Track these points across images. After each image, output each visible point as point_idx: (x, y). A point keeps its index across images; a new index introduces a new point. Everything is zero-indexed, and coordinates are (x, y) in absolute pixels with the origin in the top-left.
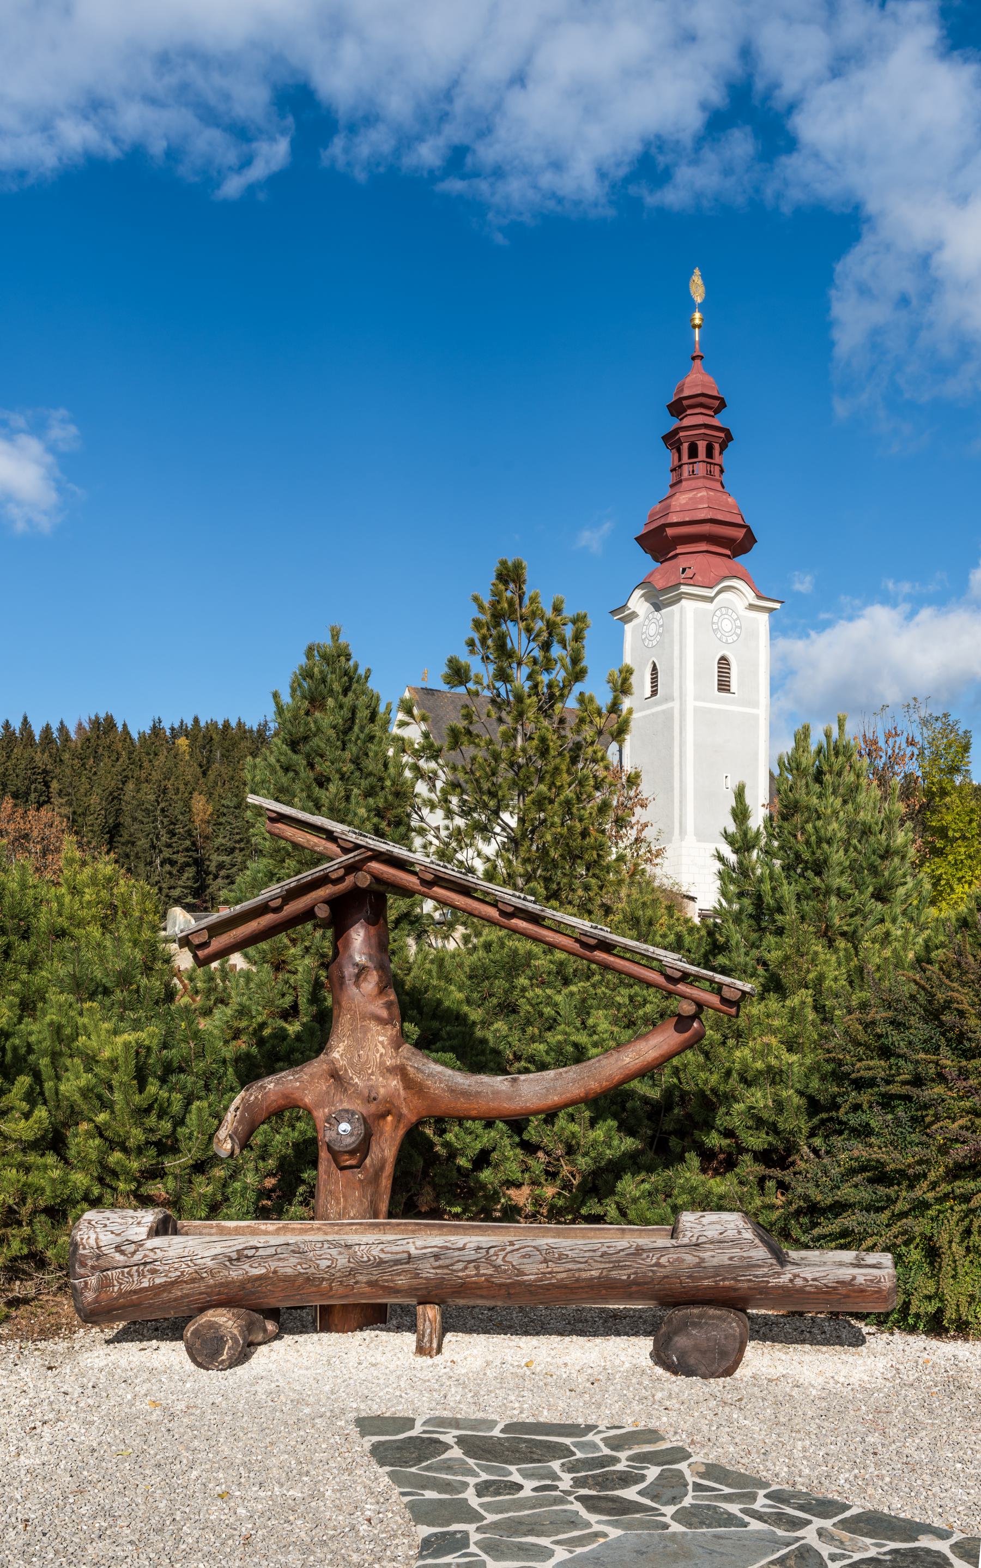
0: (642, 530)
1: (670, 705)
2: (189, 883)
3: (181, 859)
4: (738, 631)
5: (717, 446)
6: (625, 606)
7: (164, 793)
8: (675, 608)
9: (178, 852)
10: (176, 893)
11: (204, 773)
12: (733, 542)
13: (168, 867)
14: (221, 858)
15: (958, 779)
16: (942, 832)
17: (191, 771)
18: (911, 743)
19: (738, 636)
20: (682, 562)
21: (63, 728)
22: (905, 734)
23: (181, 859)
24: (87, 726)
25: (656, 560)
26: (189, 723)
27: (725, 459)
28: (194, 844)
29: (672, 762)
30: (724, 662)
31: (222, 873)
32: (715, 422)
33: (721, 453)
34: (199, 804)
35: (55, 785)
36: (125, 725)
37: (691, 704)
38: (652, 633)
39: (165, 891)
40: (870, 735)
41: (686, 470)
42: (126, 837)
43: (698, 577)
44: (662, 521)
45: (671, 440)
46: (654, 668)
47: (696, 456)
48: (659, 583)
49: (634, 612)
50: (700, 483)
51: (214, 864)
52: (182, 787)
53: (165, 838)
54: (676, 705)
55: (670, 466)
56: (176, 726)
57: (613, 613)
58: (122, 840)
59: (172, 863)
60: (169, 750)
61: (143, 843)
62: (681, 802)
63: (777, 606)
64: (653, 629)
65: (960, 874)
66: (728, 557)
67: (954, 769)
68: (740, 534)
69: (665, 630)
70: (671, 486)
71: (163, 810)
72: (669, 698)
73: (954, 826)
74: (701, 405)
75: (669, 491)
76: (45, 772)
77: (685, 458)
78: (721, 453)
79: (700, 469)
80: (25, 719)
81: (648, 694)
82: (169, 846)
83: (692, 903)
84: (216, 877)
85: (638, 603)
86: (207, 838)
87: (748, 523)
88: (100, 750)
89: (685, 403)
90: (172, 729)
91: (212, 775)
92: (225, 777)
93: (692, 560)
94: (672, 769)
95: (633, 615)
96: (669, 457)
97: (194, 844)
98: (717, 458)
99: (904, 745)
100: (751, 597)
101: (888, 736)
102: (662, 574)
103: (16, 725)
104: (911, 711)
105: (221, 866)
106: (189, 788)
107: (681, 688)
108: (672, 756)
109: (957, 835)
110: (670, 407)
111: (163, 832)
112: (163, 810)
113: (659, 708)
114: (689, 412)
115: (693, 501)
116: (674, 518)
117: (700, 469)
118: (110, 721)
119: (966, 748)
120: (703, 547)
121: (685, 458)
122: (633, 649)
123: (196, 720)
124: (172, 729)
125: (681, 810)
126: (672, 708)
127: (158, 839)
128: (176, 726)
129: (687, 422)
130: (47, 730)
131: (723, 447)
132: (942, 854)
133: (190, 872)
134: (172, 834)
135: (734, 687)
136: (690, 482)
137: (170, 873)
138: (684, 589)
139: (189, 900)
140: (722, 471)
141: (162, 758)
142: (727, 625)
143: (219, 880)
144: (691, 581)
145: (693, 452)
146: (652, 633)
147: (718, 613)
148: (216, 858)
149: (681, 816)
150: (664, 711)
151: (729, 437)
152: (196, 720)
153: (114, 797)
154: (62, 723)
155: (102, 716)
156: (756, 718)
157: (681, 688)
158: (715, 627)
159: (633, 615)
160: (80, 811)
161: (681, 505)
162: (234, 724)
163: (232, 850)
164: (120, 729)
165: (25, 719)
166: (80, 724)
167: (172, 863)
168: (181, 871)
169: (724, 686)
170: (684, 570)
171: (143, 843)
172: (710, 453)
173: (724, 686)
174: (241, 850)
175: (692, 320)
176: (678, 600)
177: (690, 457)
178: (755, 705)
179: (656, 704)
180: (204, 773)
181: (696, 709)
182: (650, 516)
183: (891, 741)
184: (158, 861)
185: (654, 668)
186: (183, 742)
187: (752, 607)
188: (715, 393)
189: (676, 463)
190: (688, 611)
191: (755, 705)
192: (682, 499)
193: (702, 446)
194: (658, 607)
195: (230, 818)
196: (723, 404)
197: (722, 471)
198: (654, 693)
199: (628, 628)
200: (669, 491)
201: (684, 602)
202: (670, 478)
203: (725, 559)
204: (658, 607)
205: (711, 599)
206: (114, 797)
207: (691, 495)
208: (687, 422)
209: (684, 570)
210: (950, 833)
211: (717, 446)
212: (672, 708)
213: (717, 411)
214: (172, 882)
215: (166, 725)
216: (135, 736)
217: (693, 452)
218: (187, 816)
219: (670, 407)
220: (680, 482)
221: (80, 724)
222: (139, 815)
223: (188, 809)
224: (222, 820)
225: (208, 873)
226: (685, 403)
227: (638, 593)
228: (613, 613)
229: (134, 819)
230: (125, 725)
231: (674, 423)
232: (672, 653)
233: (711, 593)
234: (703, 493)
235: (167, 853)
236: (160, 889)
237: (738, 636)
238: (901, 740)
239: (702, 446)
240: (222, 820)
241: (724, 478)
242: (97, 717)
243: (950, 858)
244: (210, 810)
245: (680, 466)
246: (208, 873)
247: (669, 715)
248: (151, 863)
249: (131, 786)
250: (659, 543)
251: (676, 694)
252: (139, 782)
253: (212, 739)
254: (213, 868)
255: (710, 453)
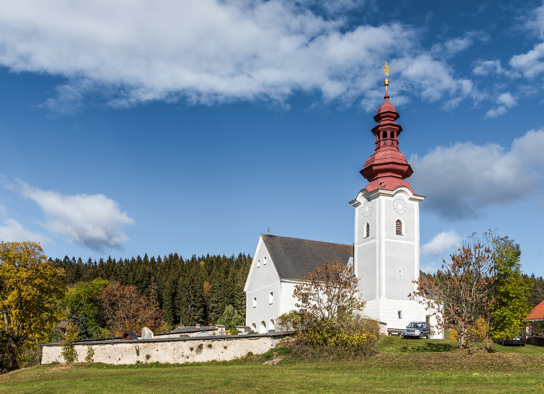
0: (363, 168)
1: (374, 240)
2: (201, 314)
3: (198, 305)
4: (405, 209)
5: (395, 133)
6: (355, 200)
7: (193, 281)
8: (377, 199)
9: (197, 303)
10: (196, 317)
11: (209, 274)
12: (404, 173)
13: (193, 308)
14: (213, 305)
15: (513, 269)
16: (506, 294)
17: (204, 273)
18: (488, 251)
19: (405, 211)
20: (380, 180)
21: (159, 258)
22: (484, 247)
23: (198, 305)
24: (168, 257)
25: (369, 181)
26: (206, 256)
27: (400, 138)
28: (203, 299)
29: (375, 265)
30: (399, 221)
31: (214, 310)
32: (395, 123)
33: (397, 136)
34: (207, 286)
35: (153, 278)
36: (181, 257)
37: (384, 240)
38: (367, 211)
39: (192, 317)
40: (466, 248)
41: (382, 143)
42: (178, 297)
43: (387, 187)
44: (371, 164)
45: (375, 131)
46: (368, 225)
47: (386, 137)
48: (370, 189)
49: (359, 202)
50: (388, 148)
51: (211, 307)
52: (200, 279)
53: (192, 298)
54: (377, 240)
55: (375, 141)
56: (201, 257)
57: (350, 203)
58: (177, 298)
59: (195, 307)
60: (197, 266)
61: (184, 299)
62: (379, 282)
63: (423, 198)
64: (367, 209)
65: (515, 315)
66: (401, 178)
67: (511, 264)
68: (405, 168)
69: (372, 209)
70: (376, 150)
71: (192, 287)
72: (374, 238)
73: (512, 292)
74: (388, 116)
75: (375, 152)
76: (150, 273)
77: (381, 138)
78: (397, 136)
79: (389, 142)
80: (146, 255)
81: (365, 236)
82: (194, 300)
83: (384, 326)
84: (212, 312)
85: (361, 198)
86: (209, 297)
87: (409, 164)
88: (171, 266)
89: (381, 115)
90: (199, 258)
91: (212, 274)
92: (217, 276)
93: (385, 180)
94: (376, 268)
95: (359, 203)
96: (375, 138)
97: (203, 299)
98: (395, 138)
99: (484, 253)
100: (411, 195)
101: (476, 248)
102: (370, 186)
103: (142, 258)
104: (488, 235)
105: (213, 308)
106: (203, 279)
107: (379, 233)
108: (375, 262)
109: (514, 296)
110: (375, 118)
111: (192, 295)
112: (192, 287)
113: (370, 242)
114: (383, 119)
115: (385, 155)
116: (376, 162)
117: (389, 142)
118: (176, 255)
119: (519, 254)
120: (390, 174)
121: (381, 138)
122: (359, 218)
123: (208, 255)
124: (199, 258)
125: (379, 285)
126: (376, 242)
127: (190, 298)
128: (201, 257)
129: (382, 123)
130: (153, 259)
131: (398, 133)
132: (506, 305)
133: (201, 310)
134: (195, 296)
135: (403, 232)
136: (383, 148)
137: (194, 310)
138: (380, 191)
139: (201, 320)
140: (398, 143)
141: (194, 268)
142: (400, 207)
143: (213, 313)
144: (384, 188)
145: (385, 135)
146: (367, 211)
147: (396, 201)
148: (212, 305)
149: (379, 288)
150: (372, 243)
151: (400, 129)
152: (208, 255)
153: (175, 283)
154: (159, 256)
155: (173, 254)
156: (413, 246)
157: (379, 233)
158: (395, 207)
159: (359, 203)
160: (162, 287)
161: (379, 157)
162: (222, 257)
163: (218, 302)
164: (179, 257)
165: (146, 255)
166: (165, 257)
167: (195, 307)
168: (198, 309)
169: (399, 232)
170: (381, 184)
171: (184, 299)
172: (392, 135)
173: (399, 232)
174: (221, 302)
175: (385, 82)
176: (378, 196)
177: (383, 138)
178: (413, 240)
179: (369, 240)
180: (209, 274)
181: (386, 242)
182: (366, 162)
183: (477, 250)
184: (190, 306)
185: (368, 225)
186: (202, 263)
187: (411, 199)
188: (394, 111)
189: (378, 140)
190: (382, 200)
191: (413, 240)
192: (380, 155)
193: (389, 133)
194: (369, 200)
195: (217, 290)
196: (398, 116)
197: (398, 143)
198: (368, 236)
199: (357, 209)
200: (375, 152)
201: (380, 197)
202: (375, 147)
203: (399, 179)
204: (369, 200)
205: (393, 196)
206: (175, 283)
207: (384, 153)
208: (382, 123)
209: (381, 184)
210: (510, 295)
211: (395, 133)
212: (376, 242)
213: (395, 119)
214: (195, 314)
215: (197, 257)
216: (185, 261)
217: (385, 135)
218: (201, 290)
219: (375, 118)
220: (379, 148)
221: (165, 257)
222: (184, 289)
223: (202, 287)
224: (214, 291)
225: (209, 310)
226: (381, 115)
227: (361, 194)
228: (350, 203)
229: (182, 291)
230: (181, 257)
231: (377, 124)
232: (376, 218)
233: (393, 193)
234: (389, 152)
235: (193, 303)
236: (190, 316)
237: (405, 211)
238: (482, 250)
239: (389, 133)
240: (214, 291)
241: (399, 146)
242: (172, 254)
243: (511, 307)
244: (210, 287)
245: (379, 142)
246: (209, 310)
247: (374, 245)
248: (187, 306)
249: (181, 278)
250: (370, 173)
251: (377, 236)
252: (184, 277)
253: (213, 262)
254: (210, 309)
255: (392, 135)
